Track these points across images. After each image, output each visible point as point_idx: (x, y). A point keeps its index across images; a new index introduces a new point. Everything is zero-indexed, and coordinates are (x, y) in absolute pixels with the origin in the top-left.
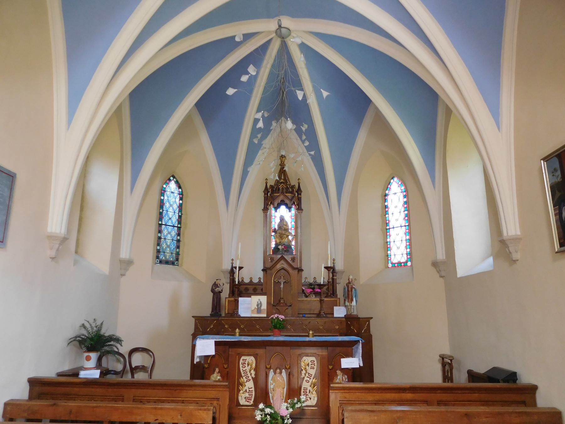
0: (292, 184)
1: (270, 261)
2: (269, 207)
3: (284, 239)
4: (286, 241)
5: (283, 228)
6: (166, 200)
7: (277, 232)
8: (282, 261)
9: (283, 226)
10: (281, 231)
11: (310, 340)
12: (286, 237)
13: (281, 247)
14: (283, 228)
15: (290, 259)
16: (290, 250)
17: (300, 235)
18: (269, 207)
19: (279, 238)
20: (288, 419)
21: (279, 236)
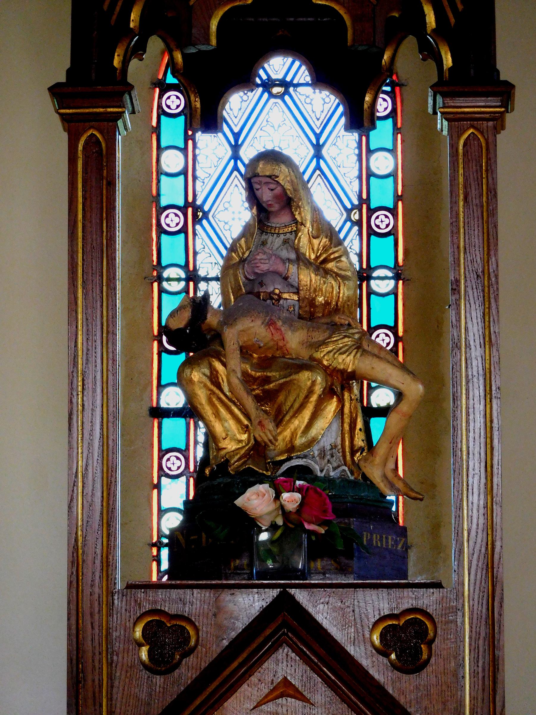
0: (307, 358)
1: (144, 654)
2: (125, 63)
3: (307, 414)
4: (326, 442)
5: (291, 297)
6: (318, 426)
7: (218, 337)
8: (284, 652)
9: (293, 269)
10: (270, 324)
11: (300, 403)
12: (318, 389)
13: (272, 507)
14: (291, 297)
15: (376, 638)
16: (313, 435)
17: (477, 365)
18: (125, 63)
19: (250, 403)
20: (302, 290)
21: (247, 379)
